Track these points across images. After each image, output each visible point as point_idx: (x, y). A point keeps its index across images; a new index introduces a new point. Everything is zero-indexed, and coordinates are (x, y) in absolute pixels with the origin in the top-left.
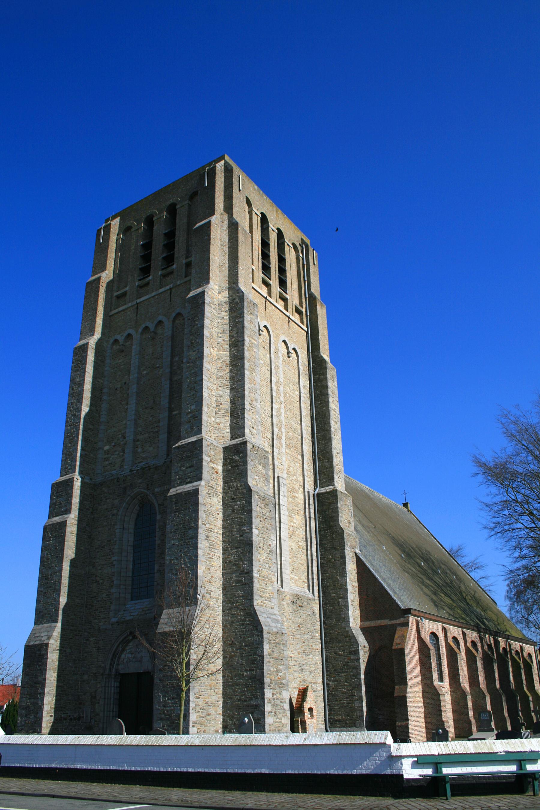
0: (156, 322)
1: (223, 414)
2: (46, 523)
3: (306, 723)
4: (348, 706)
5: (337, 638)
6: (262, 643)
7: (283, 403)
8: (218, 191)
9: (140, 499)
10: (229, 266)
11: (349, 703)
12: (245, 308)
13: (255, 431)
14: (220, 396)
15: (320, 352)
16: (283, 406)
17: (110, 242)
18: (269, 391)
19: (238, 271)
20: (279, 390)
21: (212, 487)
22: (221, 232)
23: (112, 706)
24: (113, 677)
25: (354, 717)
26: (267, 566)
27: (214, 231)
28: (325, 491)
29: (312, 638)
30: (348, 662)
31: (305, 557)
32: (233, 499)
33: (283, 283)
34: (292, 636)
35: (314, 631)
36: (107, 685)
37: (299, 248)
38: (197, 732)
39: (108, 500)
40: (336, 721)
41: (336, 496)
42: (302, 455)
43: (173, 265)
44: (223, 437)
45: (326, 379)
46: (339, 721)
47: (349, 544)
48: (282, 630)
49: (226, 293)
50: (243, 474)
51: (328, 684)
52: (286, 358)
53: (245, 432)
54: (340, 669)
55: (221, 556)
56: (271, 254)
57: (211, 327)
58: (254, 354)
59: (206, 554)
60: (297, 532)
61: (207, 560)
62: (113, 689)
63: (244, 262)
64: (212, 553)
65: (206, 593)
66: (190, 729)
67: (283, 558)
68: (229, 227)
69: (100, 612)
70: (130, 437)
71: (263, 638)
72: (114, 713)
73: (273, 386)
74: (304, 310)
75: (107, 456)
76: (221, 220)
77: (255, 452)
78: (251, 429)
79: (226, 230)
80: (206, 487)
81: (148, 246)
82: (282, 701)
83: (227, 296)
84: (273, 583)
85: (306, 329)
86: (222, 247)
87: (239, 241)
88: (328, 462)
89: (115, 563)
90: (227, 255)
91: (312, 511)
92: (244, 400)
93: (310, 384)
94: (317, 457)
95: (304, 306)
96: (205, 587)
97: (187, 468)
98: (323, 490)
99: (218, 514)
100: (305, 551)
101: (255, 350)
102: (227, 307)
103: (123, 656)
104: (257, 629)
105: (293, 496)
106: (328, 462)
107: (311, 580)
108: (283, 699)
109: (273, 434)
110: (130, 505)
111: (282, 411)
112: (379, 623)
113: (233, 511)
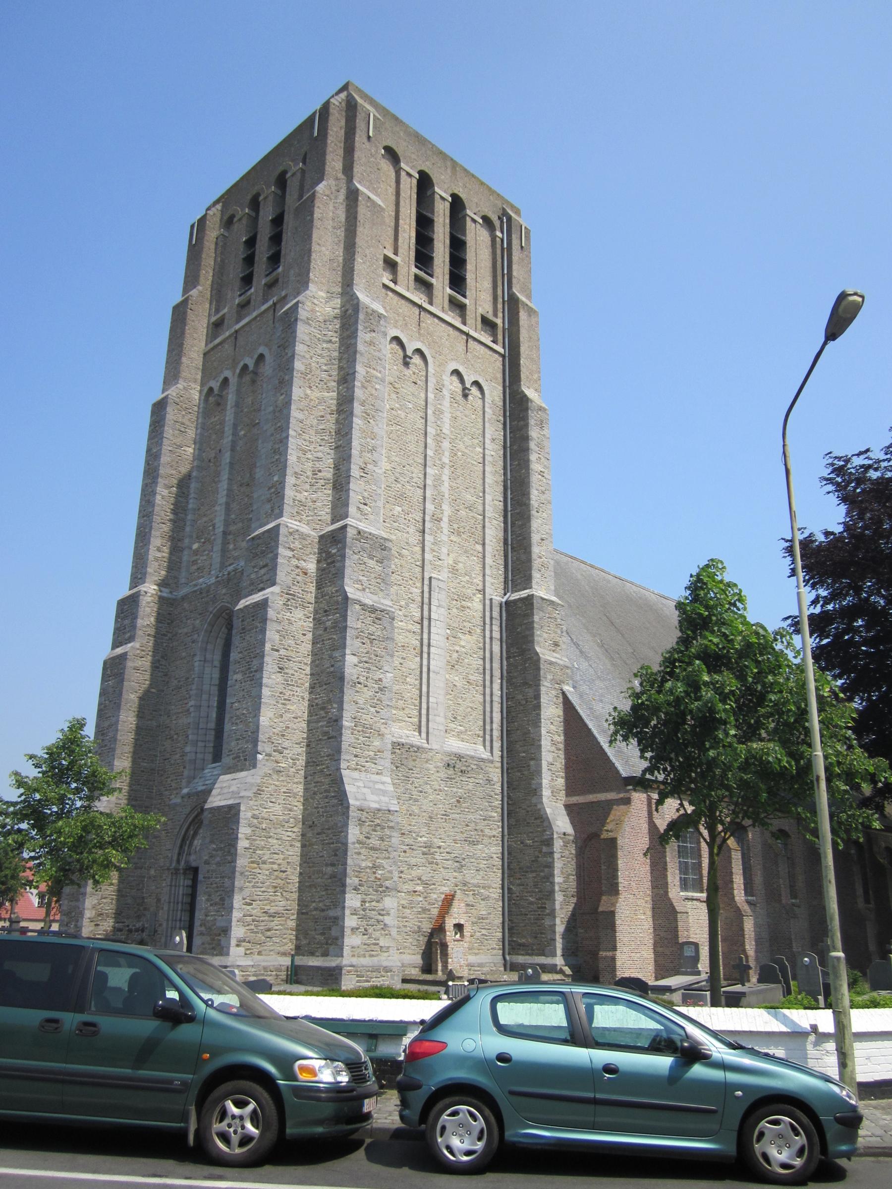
0: (256, 356)
1: (323, 486)
2: (109, 655)
3: (447, 946)
4: (536, 923)
5: (525, 820)
6: (346, 825)
7: (447, 467)
8: (332, 142)
9: (227, 617)
10: (344, 260)
11: (537, 919)
12: (360, 321)
13: (369, 509)
14: (319, 459)
15: (520, 385)
16: (447, 471)
17: (205, 242)
18: (421, 449)
19: (354, 267)
20: (440, 447)
21: (294, 596)
22: (334, 207)
23: (179, 913)
24: (182, 871)
25: (543, 940)
26: (373, 710)
27: (321, 206)
28: (518, 597)
29: (484, 820)
30: (538, 857)
31: (480, 698)
32: (326, 611)
33: (457, 281)
34: (443, 815)
35: (490, 808)
36: (173, 884)
37: (497, 223)
38: (246, 954)
39: (189, 621)
40: (520, 945)
41: (532, 604)
42: (484, 545)
43: (279, 267)
44: (320, 520)
45: (527, 425)
46: (523, 945)
47: (549, 677)
48: (390, 805)
49: (338, 302)
50: (339, 575)
51: (509, 889)
52: (460, 397)
53: (348, 511)
54: (528, 867)
55: (307, 696)
56: (435, 237)
57: (308, 356)
58: (374, 392)
59: (278, 694)
60: (466, 660)
61: (277, 702)
62: (181, 888)
63: (367, 252)
64: (289, 692)
65: (275, 751)
66: (231, 948)
67: (431, 699)
68: (347, 198)
69: (172, 781)
70: (220, 529)
71: (348, 818)
72: (182, 923)
73: (429, 441)
74: (499, 321)
75: (195, 558)
76: (336, 188)
77: (362, 541)
78: (362, 506)
79: (342, 204)
80: (282, 596)
81: (251, 242)
82: (382, 912)
83: (339, 306)
84: (383, 735)
85: (501, 350)
86: (335, 231)
87: (359, 218)
88: (524, 553)
89: (192, 709)
90: (343, 242)
91: (496, 628)
92: (350, 462)
93: (505, 436)
94: (510, 547)
95: (500, 315)
96: (273, 743)
97: (261, 569)
98: (515, 596)
99: (304, 635)
100: (481, 688)
101: (377, 386)
102: (337, 325)
103: (196, 842)
104: (342, 804)
105: (462, 606)
106: (524, 553)
107: (488, 732)
108: (383, 910)
109: (424, 513)
110: (213, 626)
111: (445, 478)
112: (591, 798)
113: (326, 629)
